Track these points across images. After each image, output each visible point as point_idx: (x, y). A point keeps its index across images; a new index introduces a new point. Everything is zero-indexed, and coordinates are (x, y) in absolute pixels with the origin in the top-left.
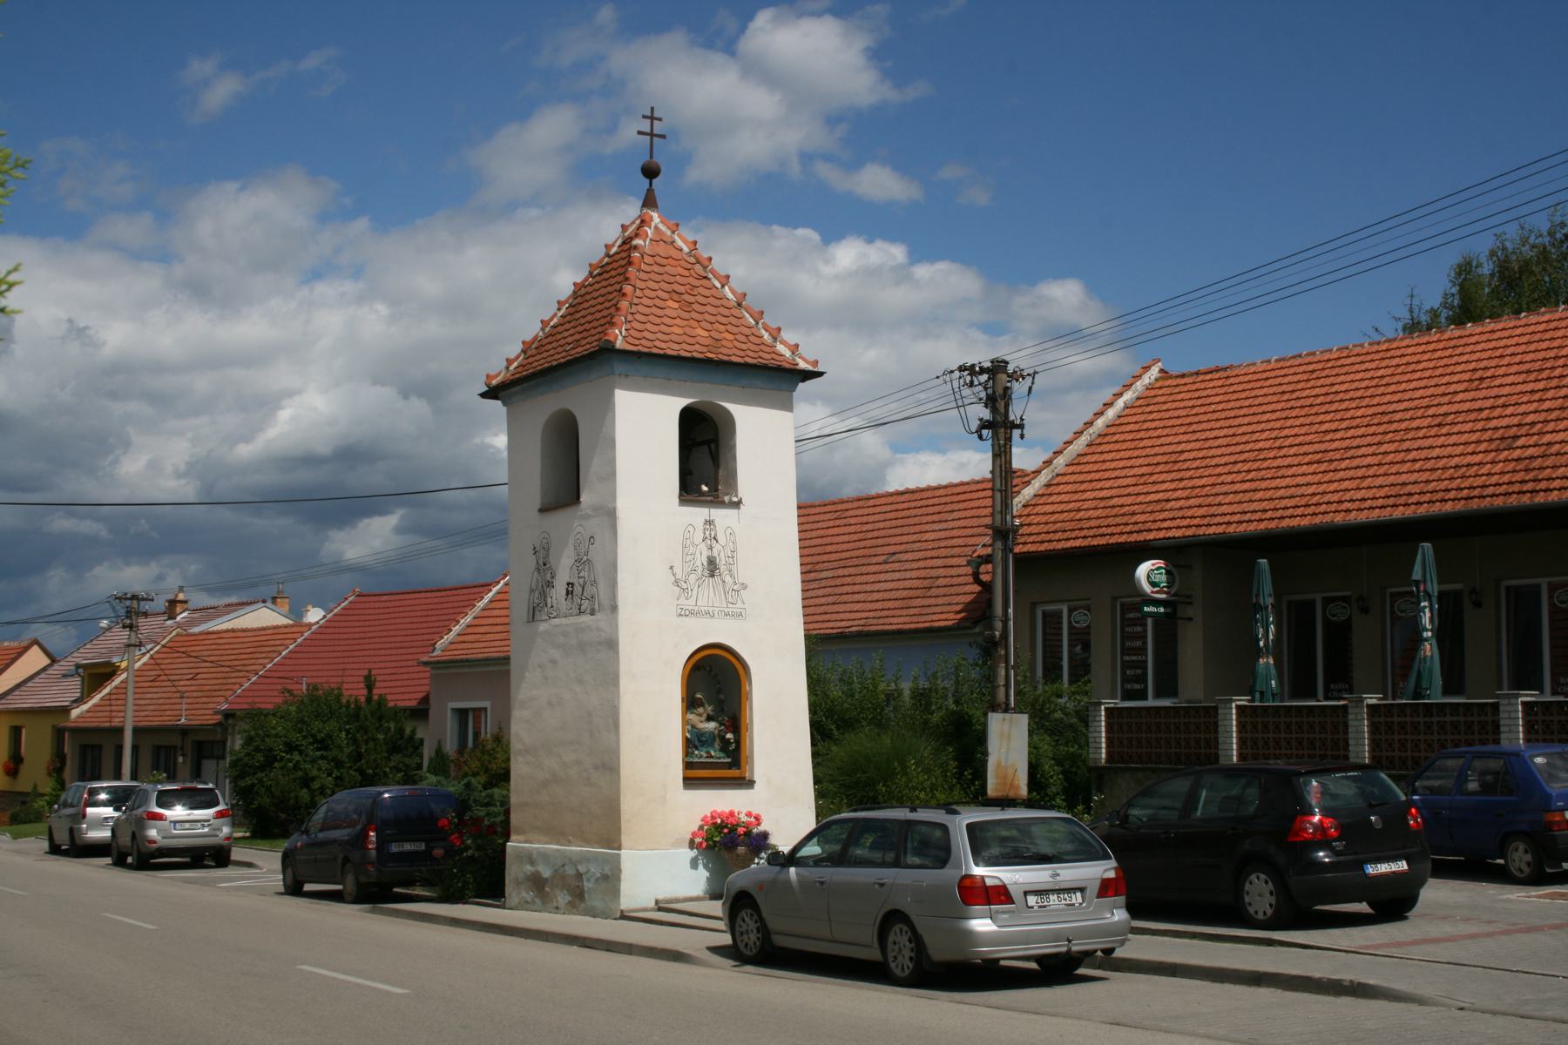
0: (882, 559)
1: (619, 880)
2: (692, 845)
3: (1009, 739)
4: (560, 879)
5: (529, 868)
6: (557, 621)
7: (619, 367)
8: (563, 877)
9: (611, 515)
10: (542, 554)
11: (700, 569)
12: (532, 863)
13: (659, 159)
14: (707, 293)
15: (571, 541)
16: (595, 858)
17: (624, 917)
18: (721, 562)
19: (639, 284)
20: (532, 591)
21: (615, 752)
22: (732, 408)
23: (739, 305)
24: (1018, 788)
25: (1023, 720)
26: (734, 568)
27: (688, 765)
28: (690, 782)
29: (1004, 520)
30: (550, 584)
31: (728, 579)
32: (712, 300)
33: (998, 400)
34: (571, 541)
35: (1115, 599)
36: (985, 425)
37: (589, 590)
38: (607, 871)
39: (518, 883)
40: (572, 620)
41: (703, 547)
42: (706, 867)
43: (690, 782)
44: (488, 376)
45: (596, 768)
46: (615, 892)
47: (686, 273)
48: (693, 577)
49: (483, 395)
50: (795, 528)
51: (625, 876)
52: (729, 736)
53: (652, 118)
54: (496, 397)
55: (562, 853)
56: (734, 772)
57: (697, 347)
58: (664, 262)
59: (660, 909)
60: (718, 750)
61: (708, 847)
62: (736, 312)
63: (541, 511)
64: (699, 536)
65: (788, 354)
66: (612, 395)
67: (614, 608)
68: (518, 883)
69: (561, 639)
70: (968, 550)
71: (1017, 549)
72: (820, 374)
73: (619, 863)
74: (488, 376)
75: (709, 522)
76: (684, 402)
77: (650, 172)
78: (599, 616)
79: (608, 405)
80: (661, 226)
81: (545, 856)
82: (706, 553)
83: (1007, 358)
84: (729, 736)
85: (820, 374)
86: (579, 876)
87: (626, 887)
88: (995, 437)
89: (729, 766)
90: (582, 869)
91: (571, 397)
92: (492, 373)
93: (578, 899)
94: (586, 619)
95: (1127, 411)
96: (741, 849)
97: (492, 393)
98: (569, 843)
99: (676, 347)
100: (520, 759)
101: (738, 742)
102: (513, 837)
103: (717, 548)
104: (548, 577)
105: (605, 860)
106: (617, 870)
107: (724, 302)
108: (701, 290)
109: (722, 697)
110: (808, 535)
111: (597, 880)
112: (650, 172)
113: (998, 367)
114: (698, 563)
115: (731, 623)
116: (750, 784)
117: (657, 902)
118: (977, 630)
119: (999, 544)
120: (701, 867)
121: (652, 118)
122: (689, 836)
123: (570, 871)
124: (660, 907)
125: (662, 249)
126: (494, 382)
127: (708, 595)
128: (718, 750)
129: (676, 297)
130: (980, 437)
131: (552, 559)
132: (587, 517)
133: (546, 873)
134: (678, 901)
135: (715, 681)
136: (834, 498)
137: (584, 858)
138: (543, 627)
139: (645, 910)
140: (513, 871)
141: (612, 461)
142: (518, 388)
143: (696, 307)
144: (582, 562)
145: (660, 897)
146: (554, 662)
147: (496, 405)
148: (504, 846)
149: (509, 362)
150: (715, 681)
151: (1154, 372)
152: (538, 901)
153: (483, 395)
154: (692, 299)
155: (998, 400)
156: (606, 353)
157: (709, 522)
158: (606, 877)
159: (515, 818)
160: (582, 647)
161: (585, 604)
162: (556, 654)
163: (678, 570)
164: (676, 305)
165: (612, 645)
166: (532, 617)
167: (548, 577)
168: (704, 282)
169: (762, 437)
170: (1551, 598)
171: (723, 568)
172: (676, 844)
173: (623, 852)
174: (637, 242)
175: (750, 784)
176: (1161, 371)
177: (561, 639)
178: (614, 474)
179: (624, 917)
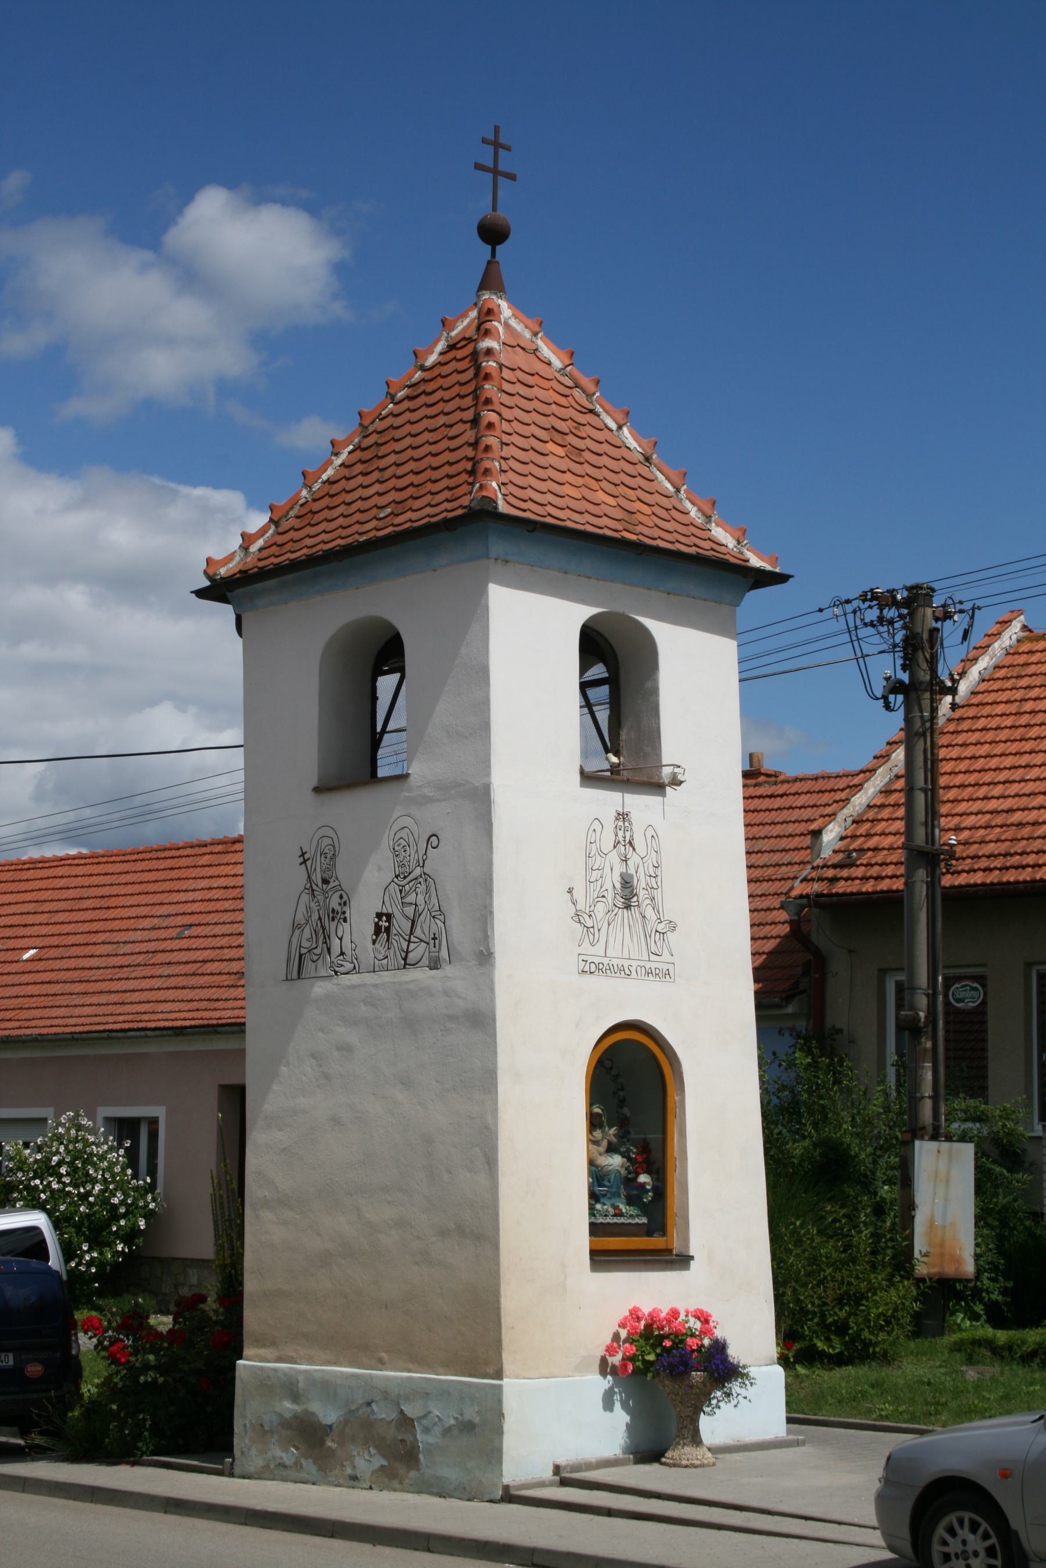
0: (173, 933)
1: (500, 1432)
2: (604, 1367)
3: (948, 1182)
4: (360, 1426)
5: (288, 1406)
6: (354, 979)
7: (497, 546)
8: (368, 1424)
9: (479, 799)
10: (318, 865)
11: (610, 896)
12: (295, 1396)
13: (505, 213)
14: (599, 436)
15: (386, 844)
16: (444, 1392)
17: (509, 1497)
18: (641, 884)
19: (507, 413)
20: (295, 926)
21: (488, 1208)
22: (658, 629)
23: (648, 459)
24: (958, 1261)
25: (967, 1151)
26: (657, 894)
27: (595, 1230)
28: (601, 1258)
29: (930, 838)
30: (339, 916)
31: (649, 913)
32: (605, 447)
33: (918, 649)
34: (386, 844)
35: (1029, 965)
36: (896, 687)
37: (426, 927)
38: (471, 1413)
39: (262, 1431)
40: (386, 976)
41: (614, 857)
42: (625, 1406)
43: (601, 1258)
44: (209, 561)
45: (444, 1233)
46: (493, 1454)
47: (562, 401)
48: (600, 909)
49: (201, 594)
50: (739, 832)
51: (510, 1424)
52: (643, 1178)
53: (497, 145)
54: (223, 599)
55: (368, 1381)
56: (655, 1242)
57: (605, 521)
58: (530, 380)
59: (564, 1483)
60: (636, 1209)
61: (636, 1372)
62: (643, 470)
63: (317, 790)
64: (607, 840)
65: (730, 542)
66: (483, 592)
67: (485, 957)
68: (262, 1431)
69: (363, 1010)
70: (784, 887)
71: (947, 881)
72: (781, 578)
73: (500, 1402)
74: (209, 561)
75: (623, 816)
76: (584, 612)
77: (493, 234)
78: (448, 970)
79: (474, 613)
80: (513, 323)
81: (327, 1388)
82: (619, 868)
83: (934, 585)
84: (643, 1178)
85: (781, 578)
86: (406, 1422)
87: (513, 1444)
88: (907, 703)
89: (649, 1231)
90: (410, 1410)
91: (388, 598)
92: (218, 556)
93: (401, 1457)
94: (421, 975)
95: (983, 686)
96: (697, 1376)
97: (217, 590)
98: (381, 1364)
99: (576, 517)
100: (267, 1215)
101: (660, 1192)
102: (247, 1352)
103: (634, 859)
104: (334, 903)
105: (466, 1394)
106: (497, 1415)
107: (624, 452)
108: (588, 430)
109: (626, 1111)
110: (759, 845)
111: (447, 1431)
112: (493, 234)
113: (918, 596)
114: (608, 885)
115: (653, 986)
116: (683, 1261)
117: (557, 1470)
118: (790, 1010)
119: (921, 874)
120: (618, 1406)
121: (497, 145)
122: (601, 1352)
123: (383, 1412)
124: (563, 1477)
125: (519, 359)
126: (223, 571)
127: (621, 940)
128: (636, 1209)
129: (558, 438)
130: (887, 707)
131: (343, 871)
132: (425, 801)
133: (329, 1415)
134: (589, 1466)
135: (631, 1083)
136: (193, 840)
137: (425, 1393)
138: (319, 989)
139: (542, 1484)
140: (248, 1410)
141: (483, 705)
142: (272, 582)
143: (587, 455)
144: (406, 878)
145: (562, 1461)
146: (346, 1049)
147: (224, 614)
148: (233, 1367)
149: (247, 539)
150: (631, 1083)
151: (1016, 627)
152: (308, 1465)
153: (201, 594)
154: (580, 444)
155: (918, 649)
156: (482, 517)
157: (623, 816)
158: (468, 1427)
159: (252, 1318)
160: (411, 1024)
161: (418, 951)
162: (352, 1036)
163: (579, 894)
164: (561, 452)
165: (481, 1021)
166: (298, 967)
167: (334, 903)
168: (590, 418)
169: (696, 671)
170: (946, 996)
171: (642, 894)
172: (580, 1369)
173: (506, 1382)
174: (487, 343)
175: (683, 1261)
176: (1025, 628)
177: (363, 1010)
178: (486, 726)
179: (509, 1497)
